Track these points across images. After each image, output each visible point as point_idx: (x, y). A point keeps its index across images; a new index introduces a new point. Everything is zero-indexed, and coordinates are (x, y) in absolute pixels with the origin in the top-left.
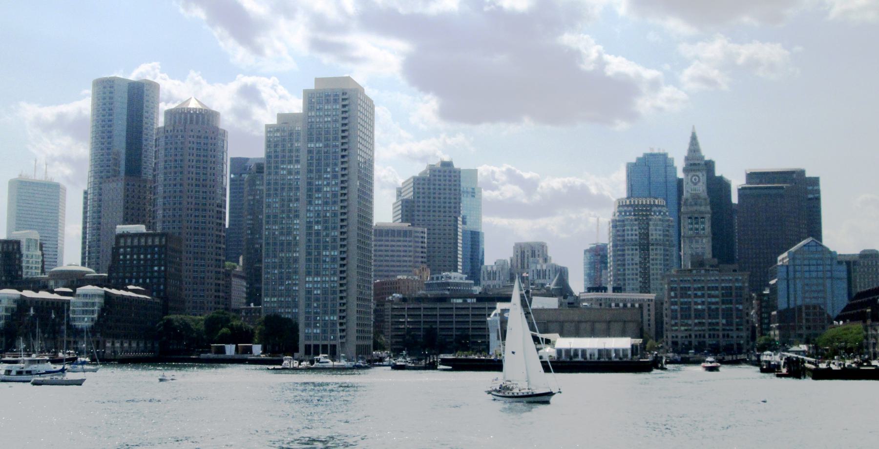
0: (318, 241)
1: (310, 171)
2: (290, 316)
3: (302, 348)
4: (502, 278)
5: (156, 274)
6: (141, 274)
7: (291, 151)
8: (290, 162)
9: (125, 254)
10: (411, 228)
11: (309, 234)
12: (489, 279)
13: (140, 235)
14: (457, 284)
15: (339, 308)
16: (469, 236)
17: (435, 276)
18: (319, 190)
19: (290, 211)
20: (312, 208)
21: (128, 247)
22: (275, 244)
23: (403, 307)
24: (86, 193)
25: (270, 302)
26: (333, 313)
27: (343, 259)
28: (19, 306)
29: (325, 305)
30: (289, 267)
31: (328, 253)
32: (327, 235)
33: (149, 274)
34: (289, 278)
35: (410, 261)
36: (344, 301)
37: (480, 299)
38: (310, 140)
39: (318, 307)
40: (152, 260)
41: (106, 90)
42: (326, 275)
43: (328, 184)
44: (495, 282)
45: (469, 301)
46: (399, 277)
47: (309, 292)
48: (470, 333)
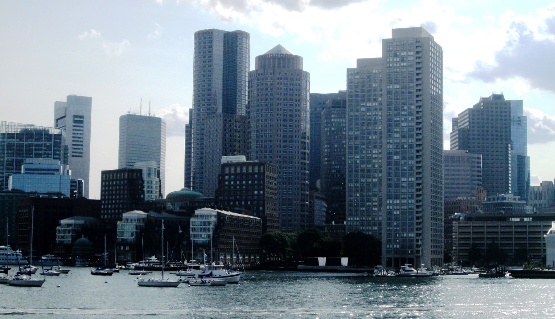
0: (397, 169)
1: (389, 109)
2: (370, 233)
3: (384, 261)
4: (547, 198)
5: (255, 197)
6: (244, 198)
7: (369, 91)
8: (369, 101)
9: (229, 181)
10: (468, 154)
11: (389, 163)
12: (536, 198)
13: (241, 165)
14: (511, 204)
15: (415, 226)
16: (516, 159)
17: (491, 197)
18: (397, 125)
19: (369, 143)
20: (391, 141)
21: (232, 174)
22: (357, 171)
23: (468, 225)
25: (351, 221)
26: (411, 231)
27: (418, 184)
28: (146, 225)
29: (404, 224)
30: (369, 191)
31: (406, 180)
32: (405, 164)
33: (250, 197)
34: (369, 201)
35: (468, 184)
36: (420, 221)
37: (536, 218)
38: (390, 82)
39: (398, 225)
40: (253, 185)
41: (204, 40)
42: (404, 198)
43: (405, 120)
44: (541, 201)
45: (526, 219)
46: (459, 198)
47: (390, 213)
48: (528, 248)
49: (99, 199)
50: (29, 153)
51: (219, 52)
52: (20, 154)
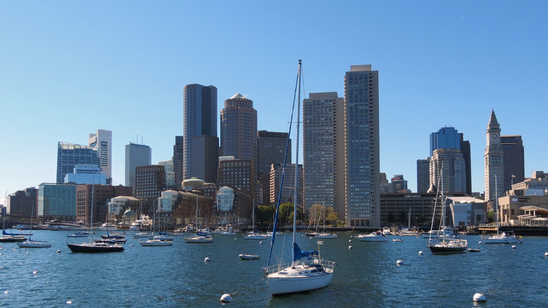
9: (226, 172)
13: (231, 161)
24: (179, 139)
49: (472, 192)
50: (77, 162)
51: (200, 99)
52: (72, 162)
